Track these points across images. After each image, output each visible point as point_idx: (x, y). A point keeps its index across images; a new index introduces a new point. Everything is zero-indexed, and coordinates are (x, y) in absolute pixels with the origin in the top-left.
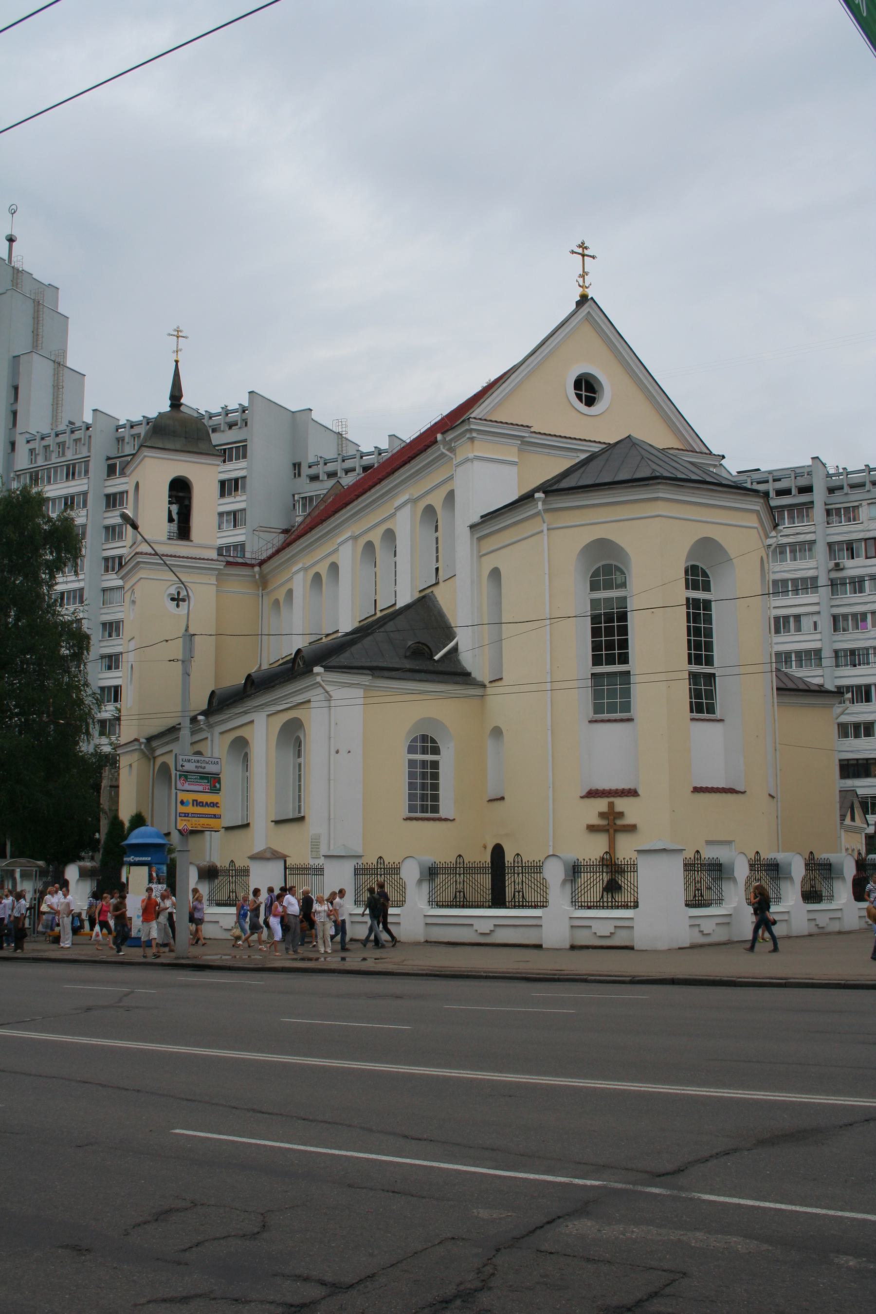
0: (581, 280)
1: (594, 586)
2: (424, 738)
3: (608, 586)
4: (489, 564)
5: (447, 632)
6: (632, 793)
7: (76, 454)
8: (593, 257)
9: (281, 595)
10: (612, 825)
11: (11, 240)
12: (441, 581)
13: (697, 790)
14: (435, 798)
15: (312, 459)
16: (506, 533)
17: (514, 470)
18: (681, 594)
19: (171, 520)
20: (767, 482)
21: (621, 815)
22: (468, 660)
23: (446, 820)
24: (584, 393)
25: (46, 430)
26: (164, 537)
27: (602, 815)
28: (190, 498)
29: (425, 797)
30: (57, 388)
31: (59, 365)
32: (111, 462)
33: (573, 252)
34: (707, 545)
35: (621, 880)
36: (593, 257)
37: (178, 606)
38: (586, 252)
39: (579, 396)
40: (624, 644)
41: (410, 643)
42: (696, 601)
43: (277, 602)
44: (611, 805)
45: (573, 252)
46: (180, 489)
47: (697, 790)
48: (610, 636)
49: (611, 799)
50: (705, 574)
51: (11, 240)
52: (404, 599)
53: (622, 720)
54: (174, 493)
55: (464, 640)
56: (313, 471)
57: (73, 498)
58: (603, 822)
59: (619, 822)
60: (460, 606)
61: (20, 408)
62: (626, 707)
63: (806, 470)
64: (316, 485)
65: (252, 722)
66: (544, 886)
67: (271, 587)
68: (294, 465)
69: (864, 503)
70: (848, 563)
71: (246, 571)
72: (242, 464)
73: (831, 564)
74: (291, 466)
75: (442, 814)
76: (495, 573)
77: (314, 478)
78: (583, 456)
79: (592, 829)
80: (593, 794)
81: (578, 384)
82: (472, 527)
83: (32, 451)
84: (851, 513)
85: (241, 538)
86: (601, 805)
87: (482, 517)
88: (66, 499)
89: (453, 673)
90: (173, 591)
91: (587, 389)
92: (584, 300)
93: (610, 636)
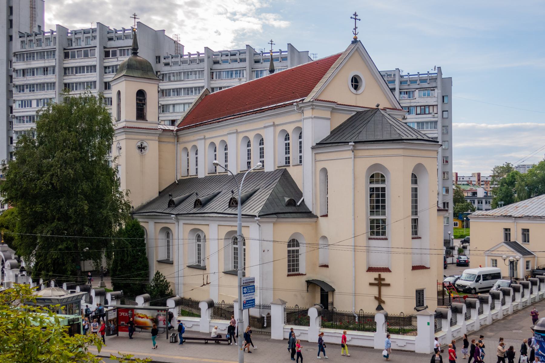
0: (354, 31)
2: (293, 240)
3: (377, 182)
5: (300, 194)
6: (387, 270)
7: (47, 46)
8: (360, 20)
10: (380, 283)
12: (291, 164)
13: (414, 268)
14: (297, 265)
15: (166, 55)
21: (384, 279)
22: (309, 205)
23: (302, 274)
24: (354, 84)
25: (29, 32)
27: (375, 279)
28: (145, 99)
29: (293, 268)
32: (66, 51)
33: (351, 18)
34: (419, 167)
35: (383, 305)
36: (360, 20)
37: (141, 151)
38: (357, 17)
39: (352, 85)
41: (287, 199)
44: (380, 275)
45: (351, 18)
47: (414, 268)
48: (378, 200)
49: (380, 273)
52: (269, 167)
54: (138, 97)
56: (167, 61)
57: (47, 68)
58: (376, 282)
59: (383, 282)
60: (304, 177)
61: (14, 18)
62: (384, 233)
65: (208, 225)
67: (181, 140)
68: (157, 57)
69: (417, 91)
70: (407, 116)
71: (171, 133)
74: (155, 58)
75: (301, 271)
76: (325, 171)
77: (167, 64)
78: (354, 113)
79: (371, 284)
80: (370, 269)
82: (313, 148)
86: (376, 275)
87: (317, 144)
88: (44, 68)
89: (308, 214)
90: (139, 144)
91: (356, 82)
92: (355, 41)
93: (378, 200)
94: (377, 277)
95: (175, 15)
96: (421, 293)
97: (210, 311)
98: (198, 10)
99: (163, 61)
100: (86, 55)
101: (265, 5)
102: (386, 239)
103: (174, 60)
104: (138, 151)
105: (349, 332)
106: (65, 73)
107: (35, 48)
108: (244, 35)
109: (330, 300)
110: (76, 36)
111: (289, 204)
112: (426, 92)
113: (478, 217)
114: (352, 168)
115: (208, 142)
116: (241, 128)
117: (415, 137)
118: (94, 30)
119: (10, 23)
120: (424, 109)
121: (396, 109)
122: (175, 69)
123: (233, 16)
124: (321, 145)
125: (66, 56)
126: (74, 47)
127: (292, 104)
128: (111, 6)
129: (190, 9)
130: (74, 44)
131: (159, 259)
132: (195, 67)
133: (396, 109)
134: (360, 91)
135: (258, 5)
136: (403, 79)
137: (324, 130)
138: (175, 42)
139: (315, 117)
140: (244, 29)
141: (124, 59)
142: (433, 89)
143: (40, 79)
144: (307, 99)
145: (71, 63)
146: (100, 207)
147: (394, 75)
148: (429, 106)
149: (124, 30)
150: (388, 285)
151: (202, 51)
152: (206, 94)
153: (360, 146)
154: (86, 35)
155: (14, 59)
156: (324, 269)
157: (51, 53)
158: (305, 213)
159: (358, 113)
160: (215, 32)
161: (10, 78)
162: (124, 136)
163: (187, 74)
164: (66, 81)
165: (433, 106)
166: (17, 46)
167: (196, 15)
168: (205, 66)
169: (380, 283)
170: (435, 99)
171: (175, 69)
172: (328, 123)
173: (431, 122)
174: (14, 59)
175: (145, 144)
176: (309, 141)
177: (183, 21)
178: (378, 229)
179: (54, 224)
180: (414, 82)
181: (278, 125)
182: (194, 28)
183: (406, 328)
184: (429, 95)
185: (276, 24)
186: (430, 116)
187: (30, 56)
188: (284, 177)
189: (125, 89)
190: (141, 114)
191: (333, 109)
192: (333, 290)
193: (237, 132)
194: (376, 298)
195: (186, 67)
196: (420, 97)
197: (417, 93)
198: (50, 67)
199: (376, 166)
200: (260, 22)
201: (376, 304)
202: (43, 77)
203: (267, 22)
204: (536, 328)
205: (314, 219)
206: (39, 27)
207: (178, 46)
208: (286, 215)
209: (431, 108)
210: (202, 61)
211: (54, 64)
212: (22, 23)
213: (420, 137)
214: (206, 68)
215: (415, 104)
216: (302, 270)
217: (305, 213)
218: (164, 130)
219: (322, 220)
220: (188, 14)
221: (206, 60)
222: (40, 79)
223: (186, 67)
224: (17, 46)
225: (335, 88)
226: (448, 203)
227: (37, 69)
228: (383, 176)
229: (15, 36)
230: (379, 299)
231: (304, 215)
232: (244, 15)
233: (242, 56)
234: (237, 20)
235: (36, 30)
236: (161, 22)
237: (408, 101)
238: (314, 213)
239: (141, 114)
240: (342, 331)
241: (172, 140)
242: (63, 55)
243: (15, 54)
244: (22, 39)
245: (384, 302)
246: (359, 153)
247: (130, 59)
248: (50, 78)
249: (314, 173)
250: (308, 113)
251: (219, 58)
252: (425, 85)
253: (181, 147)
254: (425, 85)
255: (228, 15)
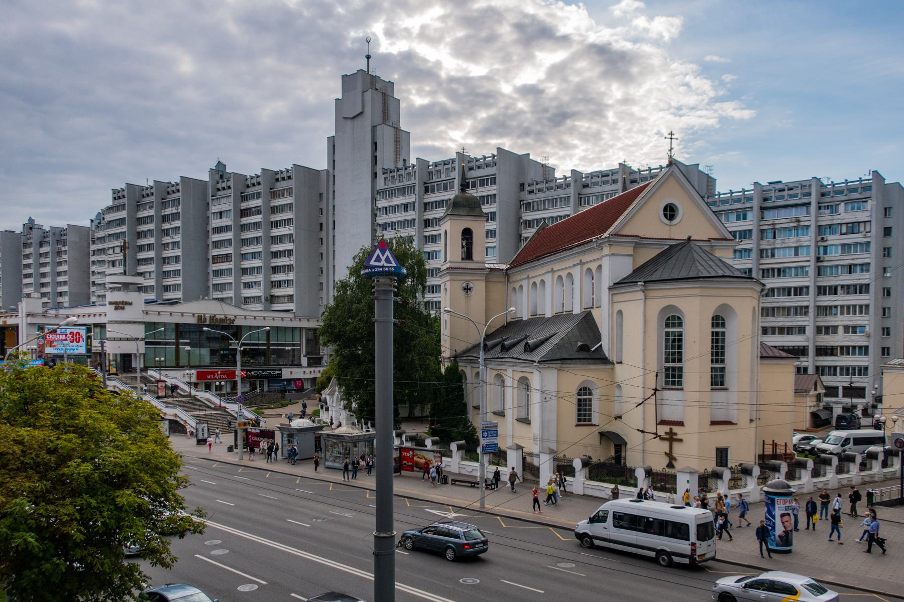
1: (667, 325)
2: (585, 388)
3: (674, 325)
4: (617, 307)
5: (598, 337)
6: (681, 424)
9: (517, 286)
11: (368, 57)
13: (713, 423)
14: (590, 415)
15: (530, 181)
16: (626, 295)
17: (631, 258)
18: (709, 329)
19: (463, 247)
20: (784, 190)
21: (676, 434)
25: (392, 168)
26: (460, 260)
27: (666, 433)
28: (471, 238)
29: (584, 415)
30: (397, 141)
31: (397, 129)
35: (674, 463)
39: (665, 216)
40: (680, 354)
41: (580, 344)
42: (717, 333)
43: (514, 288)
44: (671, 429)
46: (467, 234)
47: (713, 423)
48: (674, 347)
50: (723, 319)
51: (368, 57)
53: (678, 389)
55: (605, 343)
56: (531, 188)
60: (602, 318)
61: (379, 154)
62: (680, 383)
63: (808, 184)
64: (532, 196)
66: (636, 479)
67: (511, 280)
69: (843, 204)
72: (494, 187)
73: (819, 238)
76: (620, 312)
77: (531, 192)
78: (666, 247)
81: (665, 209)
82: (610, 289)
83: (385, 179)
84: (833, 208)
85: (494, 227)
89: (601, 359)
90: (464, 285)
91: (670, 212)
93: (674, 347)
94: (668, 431)
95: (605, 117)
96: (724, 452)
97: (585, 471)
98: (635, 109)
99: (527, 188)
100: (445, 189)
101: (721, 93)
102: (682, 389)
103: (538, 187)
104: (463, 293)
105: (620, 487)
106: (425, 209)
107: (398, 184)
108: (694, 133)
109: (623, 454)
110: (437, 168)
111: (584, 345)
112: (856, 205)
113: (894, 367)
114: (642, 310)
115: (531, 281)
116: (556, 267)
117: (720, 273)
118: (453, 161)
119: (375, 159)
120: (853, 228)
121: (726, 239)
122: (541, 196)
123: (678, 111)
124: (619, 285)
125: (427, 190)
126: (434, 180)
127: (591, 241)
128: (529, 116)
129: (623, 108)
130: (434, 177)
131: (475, 405)
132: (560, 193)
133: (726, 239)
134: (675, 222)
135: (712, 94)
136: (825, 190)
137: (626, 267)
138: (543, 165)
139: (613, 255)
140: (693, 127)
141: (451, 195)
142: (865, 200)
143: (401, 216)
144: (606, 235)
145: (431, 198)
146: (409, 351)
147: (810, 186)
148: (859, 222)
149: (485, 158)
150: (681, 440)
151: (569, 174)
152: (543, 228)
153: (651, 286)
154: (446, 167)
155: (378, 197)
156: (618, 421)
157: (411, 189)
158: (600, 359)
159: (671, 246)
160: (657, 134)
161: (374, 216)
162: (448, 278)
163: (553, 202)
164: (426, 217)
165: (865, 222)
166: (381, 184)
167: (632, 115)
168: (571, 191)
169: (671, 438)
170: (868, 214)
171: (541, 196)
172: (630, 260)
173: (862, 244)
174: (378, 197)
175: (471, 285)
176: (606, 280)
177: (615, 124)
178: (673, 377)
179: (363, 367)
180: (840, 192)
181: (585, 263)
182: (629, 131)
183: (668, 486)
184: (859, 209)
185: (738, 114)
186: (860, 235)
187: (392, 193)
188: (587, 322)
189: (450, 229)
190: (468, 255)
191: (636, 243)
192: (626, 444)
193: (553, 271)
194: (666, 453)
195: (551, 194)
196: (846, 211)
197: (842, 207)
198: (410, 203)
199: (670, 307)
200: (716, 115)
201: (666, 461)
202: (404, 214)
203: (724, 114)
204: (766, 489)
205: (610, 366)
206: (404, 160)
207: (547, 171)
208: (574, 361)
209: (862, 225)
210: (568, 185)
211: (413, 200)
212: (386, 160)
213: (728, 273)
214: (572, 194)
215: (838, 222)
216: (595, 419)
217: (600, 359)
218: (491, 269)
219: (617, 366)
220: (621, 116)
221: (572, 185)
222: (401, 216)
223: (551, 194)
224: (381, 184)
225: (645, 221)
226: (888, 348)
227: (398, 206)
228: (679, 318)
229: (380, 173)
230: (670, 455)
231: (590, 361)
232: (693, 108)
233: (614, 177)
234: (683, 115)
235: (400, 165)
236: (589, 128)
237: (830, 218)
238: (610, 358)
239: (468, 255)
240: (613, 486)
241: (502, 280)
242: (423, 190)
243: (378, 192)
244: (385, 176)
245: (675, 459)
246: (651, 294)
247: (456, 197)
248: (411, 215)
249: (611, 315)
250: (606, 250)
251: (589, 181)
252: (856, 195)
253: (510, 287)
254: (856, 195)
255: (672, 110)
